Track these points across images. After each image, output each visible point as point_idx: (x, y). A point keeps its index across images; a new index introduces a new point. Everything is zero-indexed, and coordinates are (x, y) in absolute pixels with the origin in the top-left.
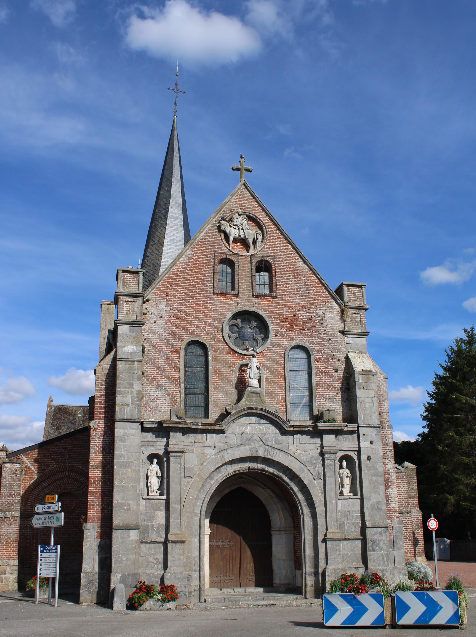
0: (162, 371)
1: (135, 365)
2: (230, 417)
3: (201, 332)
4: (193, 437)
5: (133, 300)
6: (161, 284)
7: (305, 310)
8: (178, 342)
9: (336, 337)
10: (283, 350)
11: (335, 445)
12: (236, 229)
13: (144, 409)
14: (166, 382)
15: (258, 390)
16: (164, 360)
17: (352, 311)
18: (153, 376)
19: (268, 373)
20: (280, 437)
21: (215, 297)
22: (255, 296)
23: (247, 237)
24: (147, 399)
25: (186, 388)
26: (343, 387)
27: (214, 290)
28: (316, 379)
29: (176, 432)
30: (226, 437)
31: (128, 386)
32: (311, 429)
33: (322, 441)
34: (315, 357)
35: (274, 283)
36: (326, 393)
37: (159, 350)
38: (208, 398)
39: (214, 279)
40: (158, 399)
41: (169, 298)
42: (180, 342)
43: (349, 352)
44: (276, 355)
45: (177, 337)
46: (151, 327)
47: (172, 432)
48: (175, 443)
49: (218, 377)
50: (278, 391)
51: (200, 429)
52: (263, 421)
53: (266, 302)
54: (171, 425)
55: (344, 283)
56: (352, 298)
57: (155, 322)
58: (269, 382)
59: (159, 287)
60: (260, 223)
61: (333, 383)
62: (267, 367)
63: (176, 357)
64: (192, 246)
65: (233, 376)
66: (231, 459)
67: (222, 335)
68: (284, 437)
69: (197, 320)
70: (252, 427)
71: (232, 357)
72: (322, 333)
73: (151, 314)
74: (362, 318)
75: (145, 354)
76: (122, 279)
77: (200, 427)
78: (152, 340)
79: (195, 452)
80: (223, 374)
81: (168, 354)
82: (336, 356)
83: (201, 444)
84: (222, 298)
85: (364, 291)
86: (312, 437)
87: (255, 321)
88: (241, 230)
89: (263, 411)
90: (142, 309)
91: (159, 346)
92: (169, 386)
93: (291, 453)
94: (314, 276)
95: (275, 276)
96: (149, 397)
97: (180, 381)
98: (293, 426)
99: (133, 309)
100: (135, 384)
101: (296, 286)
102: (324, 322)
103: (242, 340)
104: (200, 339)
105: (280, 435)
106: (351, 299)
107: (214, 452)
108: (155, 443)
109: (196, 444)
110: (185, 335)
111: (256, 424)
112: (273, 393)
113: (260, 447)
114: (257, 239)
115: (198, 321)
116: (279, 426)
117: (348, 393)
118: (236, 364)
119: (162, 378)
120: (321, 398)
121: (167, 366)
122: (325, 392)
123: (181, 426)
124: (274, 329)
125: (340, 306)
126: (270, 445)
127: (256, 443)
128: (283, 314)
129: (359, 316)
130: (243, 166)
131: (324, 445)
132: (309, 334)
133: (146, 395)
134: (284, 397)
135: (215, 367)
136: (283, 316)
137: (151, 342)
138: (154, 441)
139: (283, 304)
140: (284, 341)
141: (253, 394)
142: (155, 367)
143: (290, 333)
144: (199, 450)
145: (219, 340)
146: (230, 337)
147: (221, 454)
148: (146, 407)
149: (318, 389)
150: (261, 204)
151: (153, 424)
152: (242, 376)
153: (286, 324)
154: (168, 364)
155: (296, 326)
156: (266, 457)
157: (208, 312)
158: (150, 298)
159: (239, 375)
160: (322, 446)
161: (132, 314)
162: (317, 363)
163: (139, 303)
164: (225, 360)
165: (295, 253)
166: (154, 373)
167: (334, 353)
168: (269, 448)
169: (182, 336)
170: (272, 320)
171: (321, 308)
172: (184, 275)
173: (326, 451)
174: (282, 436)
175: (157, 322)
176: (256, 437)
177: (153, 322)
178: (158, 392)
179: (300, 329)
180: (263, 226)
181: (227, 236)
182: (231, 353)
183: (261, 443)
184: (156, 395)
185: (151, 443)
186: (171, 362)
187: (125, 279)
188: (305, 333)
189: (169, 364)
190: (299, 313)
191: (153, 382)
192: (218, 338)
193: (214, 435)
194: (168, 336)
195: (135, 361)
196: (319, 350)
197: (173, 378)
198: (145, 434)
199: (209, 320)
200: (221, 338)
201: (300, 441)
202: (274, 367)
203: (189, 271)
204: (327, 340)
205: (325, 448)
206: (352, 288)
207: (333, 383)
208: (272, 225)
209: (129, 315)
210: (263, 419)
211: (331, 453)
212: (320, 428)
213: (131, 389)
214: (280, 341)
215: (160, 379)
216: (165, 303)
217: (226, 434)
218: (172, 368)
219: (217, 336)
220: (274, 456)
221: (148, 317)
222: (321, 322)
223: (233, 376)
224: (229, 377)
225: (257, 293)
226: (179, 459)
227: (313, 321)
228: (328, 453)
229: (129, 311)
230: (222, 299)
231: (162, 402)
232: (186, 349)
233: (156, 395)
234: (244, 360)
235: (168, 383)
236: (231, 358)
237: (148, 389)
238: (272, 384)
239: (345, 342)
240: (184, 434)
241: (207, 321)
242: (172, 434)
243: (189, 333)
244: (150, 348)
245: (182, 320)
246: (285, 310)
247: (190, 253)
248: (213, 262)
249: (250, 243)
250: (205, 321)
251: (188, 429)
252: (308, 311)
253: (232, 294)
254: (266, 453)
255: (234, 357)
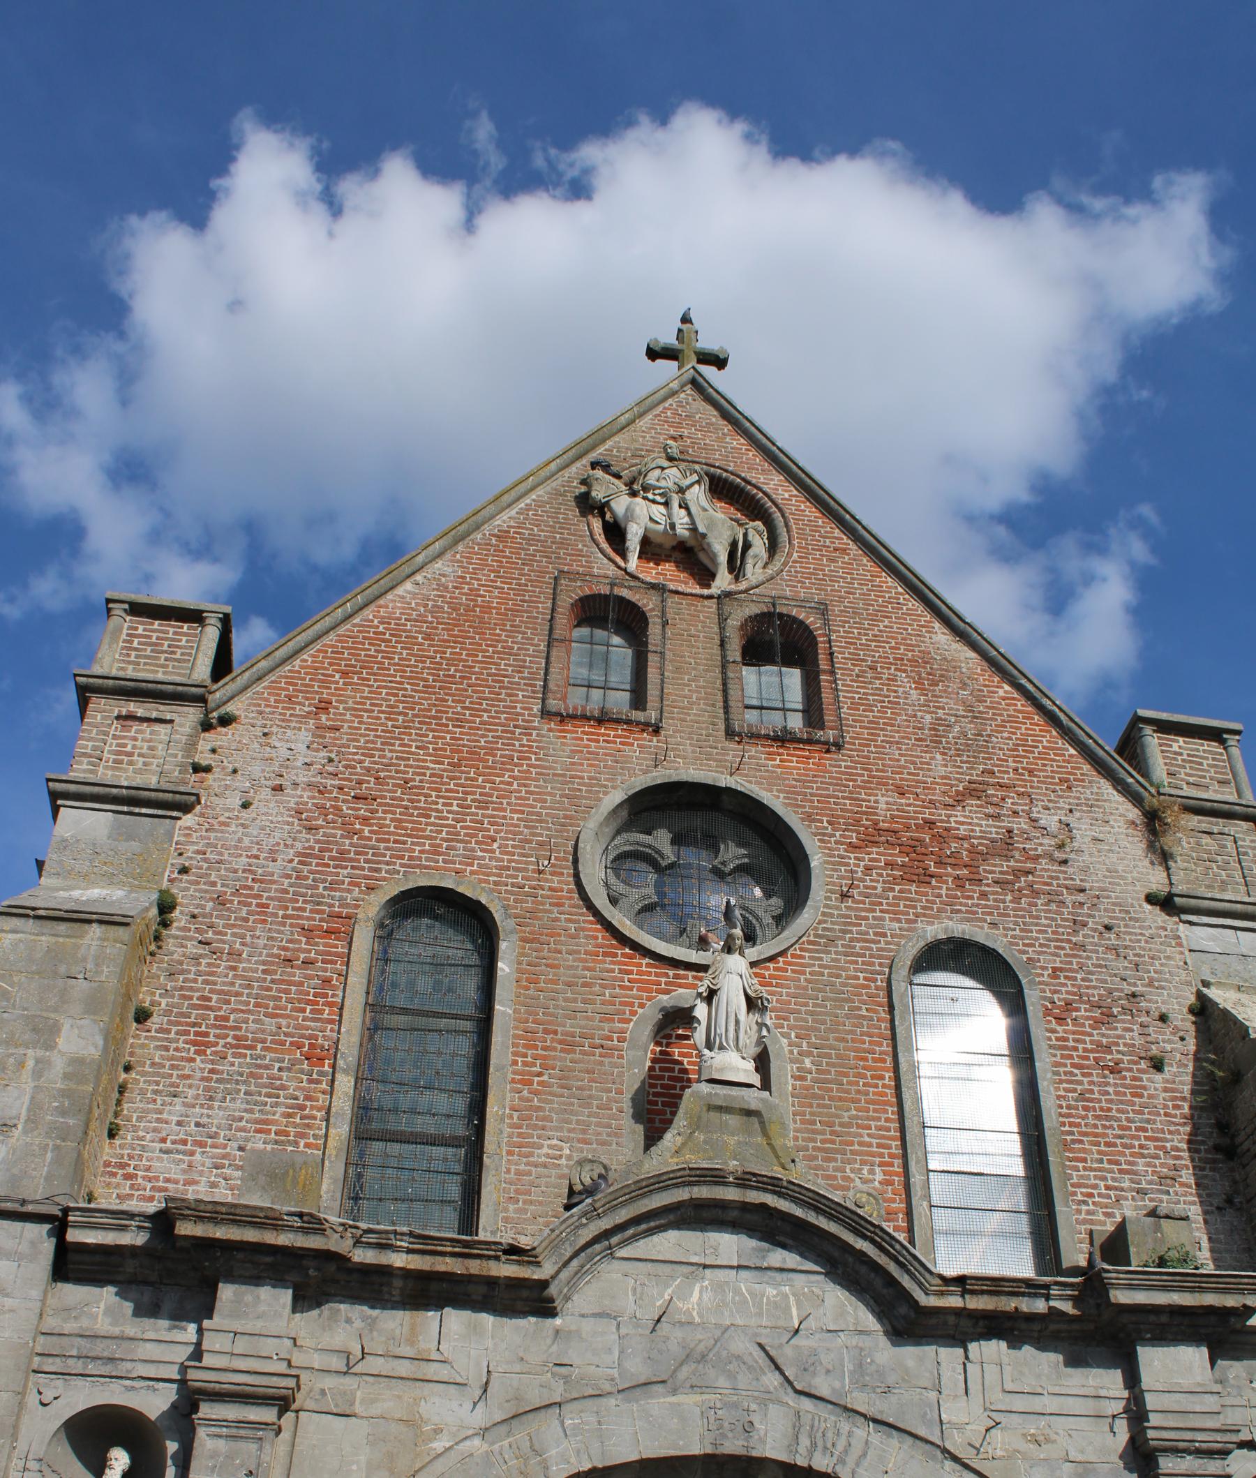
0: (249, 1012)
1: (86, 940)
2: (585, 1214)
3: (470, 859)
4: (358, 1324)
5: (154, 715)
6: (301, 667)
7: (978, 806)
8: (349, 891)
9: (1137, 920)
10: (880, 957)
11: (1211, 1403)
12: (654, 502)
13: (118, 1186)
14: (259, 1066)
15: (753, 1098)
16: (264, 963)
17: (1194, 821)
18: (197, 1034)
19: (809, 1054)
20: (884, 1352)
21: (550, 730)
22: (739, 735)
23: (702, 529)
24: (142, 1138)
25: (363, 1110)
26: (1203, 1142)
27: (544, 700)
28: (1059, 1097)
29: (255, 1280)
30: (557, 1332)
31: (28, 1036)
32: (1067, 1307)
33: (1132, 1379)
34: (1045, 998)
35: (826, 696)
36: (1117, 1163)
37: (246, 920)
38: (482, 1153)
39: (547, 663)
40: (201, 1144)
41: (328, 719)
42: (361, 892)
43: (1206, 984)
44: (848, 978)
45: (345, 872)
46: (221, 824)
47: (232, 1278)
48: (241, 1345)
49: (544, 1058)
50: (860, 1144)
51: (406, 1273)
52: (779, 1257)
53: (792, 763)
54: (220, 1233)
55: (1142, 713)
56: (1186, 774)
57: (245, 806)
58: (814, 1096)
59: (287, 677)
60: (758, 501)
61: (1148, 1121)
62: (801, 1028)
63: (329, 954)
64: (460, 547)
65: (621, 1057)
66: (586, 1466)
67: (577, 876)
68: (910, 1354)
69: (455, 808)
70: (719, 1288)
71: (621, 971)
72: (1069, 899)
73: (235, 771)
74: (1245, 854)
75: (174, 932)
76: (124, 637)
77: (398, 1260)
78: (220, 877)
79: (358, 1409)
80: (568, 1045)
81: (290, 941)
82: (1149, 1001)
83: (404, 1368)
84: (583, 732)
85: (1235, 751)
86: (1075, 1361)
87: (741, 844)
88: (675, 504)
89: (780, 1195)
90: (191, 746)
91: (250, 904)
92: (271, 1086)
93: (955, 1443)
94: (1007, 688)
95: (833, 673)
96: (155, 1130)
97: (334, 1066)
98: (961, 1280)
99: (150, 748)
100: (66, 1028)
101: (928, 717)
102: (1073, 856)
103: (673, 916)
104: (459, 884)
105: (883, 1341)
106: (1182, 780)
107: (480, 1417)
108: (126, 1344)
109: (374, 1365)
110: (388, 863)
111: (744, 1274)
112: (837, 1151)
113: (763, 1403)
114: (747, 546)
115: (458, 812)
116: (878, 1282)
117: (1232, 1170)
118: (642, 1006)
119: (240, 1043)
120: (1095, 1187)
121: (279, 991)
122: (1110, 1162)
123: (283, 1239)
124: (836, 870)
125: (1136, 799)
126: (824, 1392)
127: (744, 1380)
128: (876, 814)
129: (1230, 845)
130: (688, 345)
131: (1151, 1401)
132: (1004, 901)
133: (139, 1119)
134: (897, 1174)
135: (527, 1012)
136: (876, 823)
137: (214, 884)
138: (122, 1338)
139: (874, 777)
140: (882, 919)
141: (726, 1117)
142: (211, 991)
143: (913, 888)
144: (389, 1401)
145: (560, 898)
146: (614, 901)
147: (520, 1435)
148: (128, 1177)
149: (1074, 1141)
150: (764, 441)
151: (123, 1228)
152: (672, 1070)
153: (891, 855)
154: (281, 982)
155: (939, 863)
156: (801, 1462)
157: (510, 784)
158: (237, 713)
159: (654, 1061)
160: (1136, 1413)
161: (140, 765)
162: (1054, 1025)
163: (181, 725)
164: (585, 985)
165: (913, 604)
166: (205, 1018)
167: (1135, 985)
168: (823, 1410)
169: (371, 869)
170: (824, 835)
171: (1051, 805)
172: (410, 643)
173: (1165, 1435)
174: (894, 1344)
175: (256, 803)
176: (742, 1345)
177: (236, 802)
178: (210, 1108)
179: (957, 878)
180: (774, 509)
181: (615, 533)
182: (615, 955)
183: (772, 1379)
184: (198, 1124)
185: (100, 1348)
186: (298, 975)
187: (136, 641)
188: (983, 895)
189: (290, 983)
190: (949, 816)
191: (193, 1060)
192: (551, 889)
193: (487, 1319)
194: (301, 863)
195: (89, 922)
196: (1061, 970)
197: (299, 1046)
198: (72, 1293)
199: (512, 811)
200: (569, 891)
201: (1007, 1377)
202: (837, 1031)
203: (436, 628)
204: (1095, 930)
205: (1154, 1420)
206: (1181, 739)
207: (1148, 1121)
208: (810, 511)
209: (126, 771)
210: (784, 1246)
211: (1198, 1452)
212: (1121, 1297)
213: (40, 1053)
214: (866, 918)
215: (232, 1046)
216: (305, 736)
217: (558, 1321)
218: (300, 1001)
219: (547, 880)
220: (851, 1460)
221: (215, 784)
222: (1057, 854)
223: (621, 1057)
224: (601, 1063)
225: (750, 726)
226: (253, 1447)
227: (1017, 849)
228: (1176, 1451)
229: (130, 754)
230: (582, 739)
231: (224, 1157)
232: (385, 934)
233: (198, 1124)
234: (681, 990)
235: (267, 1067)
236: (615, 979)
237: (155, 1092)
238: (829, 1107)
239: (1180, 945)
240: (305, 1300)
241: (504, 818)
242: (227, 1292)
243: (411, 858)
244: (203, 907)
245: (380, 805)
246: (883, 800)
247: (448, 570)
248: (549, 605)
249: (713, 558)
250: (493, 816)
251: (332, 1267)
252: (990, 810)
253: (628, 722)
254: (805, 1441)
255: (631, 972)
